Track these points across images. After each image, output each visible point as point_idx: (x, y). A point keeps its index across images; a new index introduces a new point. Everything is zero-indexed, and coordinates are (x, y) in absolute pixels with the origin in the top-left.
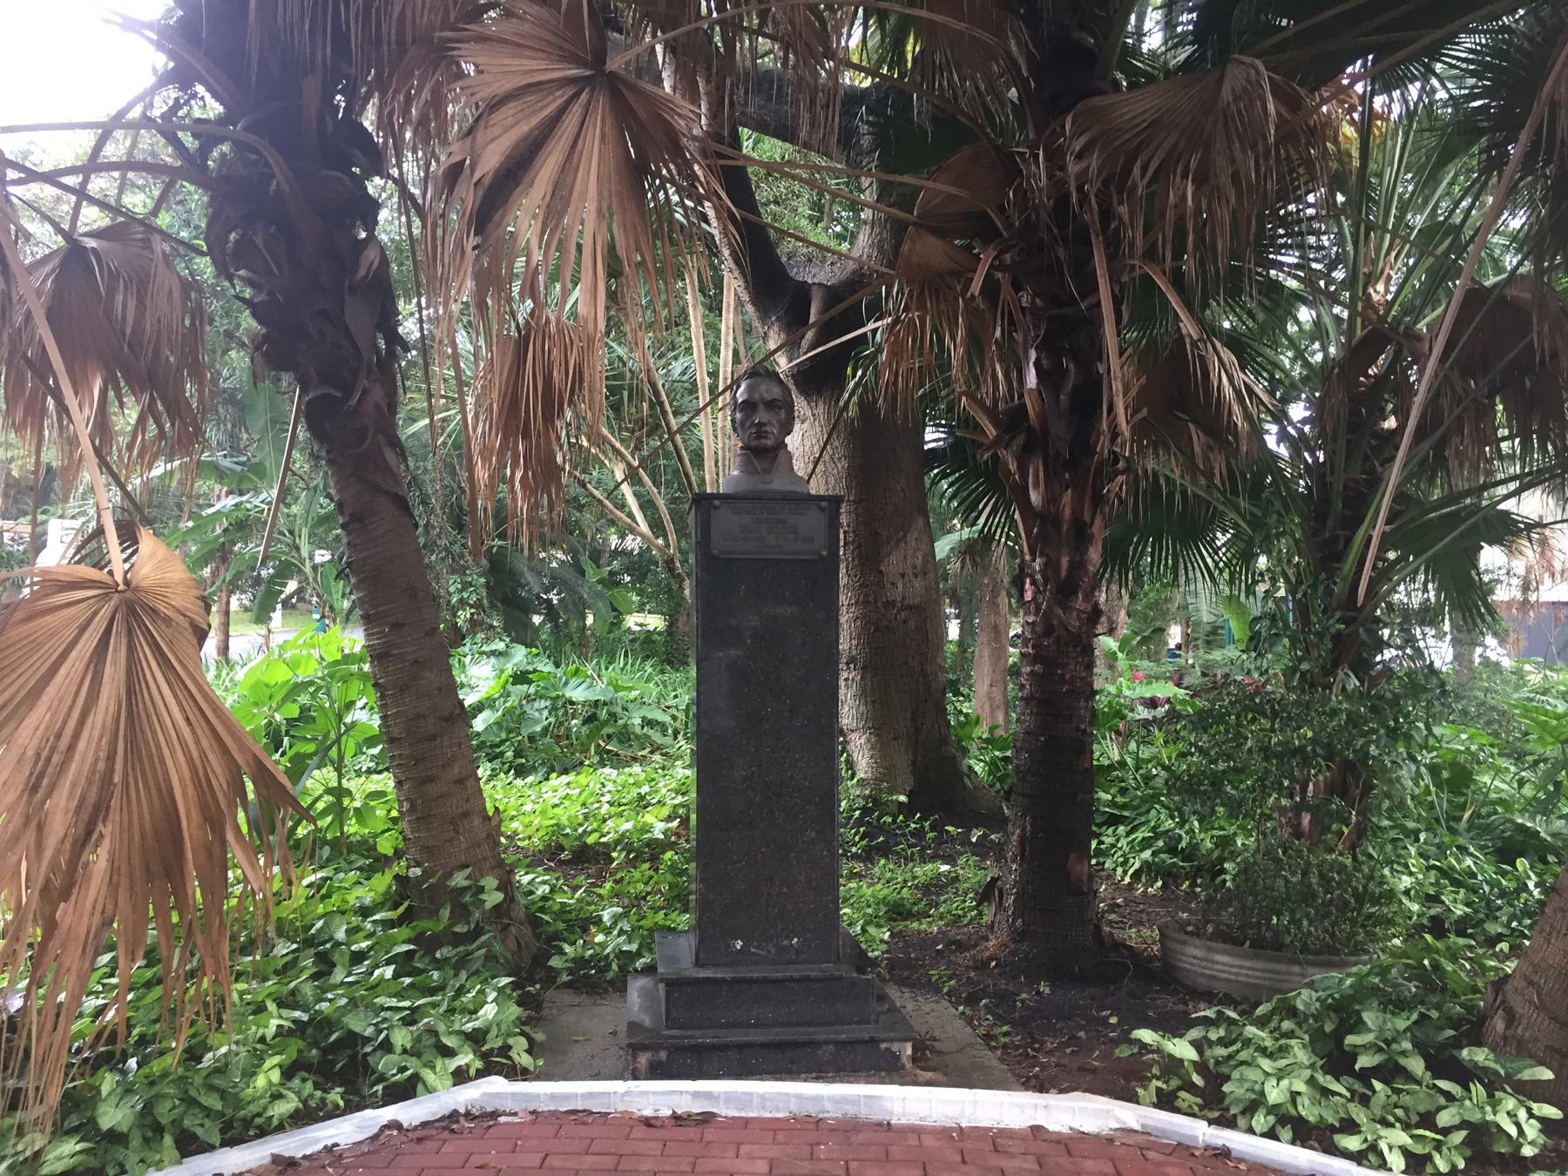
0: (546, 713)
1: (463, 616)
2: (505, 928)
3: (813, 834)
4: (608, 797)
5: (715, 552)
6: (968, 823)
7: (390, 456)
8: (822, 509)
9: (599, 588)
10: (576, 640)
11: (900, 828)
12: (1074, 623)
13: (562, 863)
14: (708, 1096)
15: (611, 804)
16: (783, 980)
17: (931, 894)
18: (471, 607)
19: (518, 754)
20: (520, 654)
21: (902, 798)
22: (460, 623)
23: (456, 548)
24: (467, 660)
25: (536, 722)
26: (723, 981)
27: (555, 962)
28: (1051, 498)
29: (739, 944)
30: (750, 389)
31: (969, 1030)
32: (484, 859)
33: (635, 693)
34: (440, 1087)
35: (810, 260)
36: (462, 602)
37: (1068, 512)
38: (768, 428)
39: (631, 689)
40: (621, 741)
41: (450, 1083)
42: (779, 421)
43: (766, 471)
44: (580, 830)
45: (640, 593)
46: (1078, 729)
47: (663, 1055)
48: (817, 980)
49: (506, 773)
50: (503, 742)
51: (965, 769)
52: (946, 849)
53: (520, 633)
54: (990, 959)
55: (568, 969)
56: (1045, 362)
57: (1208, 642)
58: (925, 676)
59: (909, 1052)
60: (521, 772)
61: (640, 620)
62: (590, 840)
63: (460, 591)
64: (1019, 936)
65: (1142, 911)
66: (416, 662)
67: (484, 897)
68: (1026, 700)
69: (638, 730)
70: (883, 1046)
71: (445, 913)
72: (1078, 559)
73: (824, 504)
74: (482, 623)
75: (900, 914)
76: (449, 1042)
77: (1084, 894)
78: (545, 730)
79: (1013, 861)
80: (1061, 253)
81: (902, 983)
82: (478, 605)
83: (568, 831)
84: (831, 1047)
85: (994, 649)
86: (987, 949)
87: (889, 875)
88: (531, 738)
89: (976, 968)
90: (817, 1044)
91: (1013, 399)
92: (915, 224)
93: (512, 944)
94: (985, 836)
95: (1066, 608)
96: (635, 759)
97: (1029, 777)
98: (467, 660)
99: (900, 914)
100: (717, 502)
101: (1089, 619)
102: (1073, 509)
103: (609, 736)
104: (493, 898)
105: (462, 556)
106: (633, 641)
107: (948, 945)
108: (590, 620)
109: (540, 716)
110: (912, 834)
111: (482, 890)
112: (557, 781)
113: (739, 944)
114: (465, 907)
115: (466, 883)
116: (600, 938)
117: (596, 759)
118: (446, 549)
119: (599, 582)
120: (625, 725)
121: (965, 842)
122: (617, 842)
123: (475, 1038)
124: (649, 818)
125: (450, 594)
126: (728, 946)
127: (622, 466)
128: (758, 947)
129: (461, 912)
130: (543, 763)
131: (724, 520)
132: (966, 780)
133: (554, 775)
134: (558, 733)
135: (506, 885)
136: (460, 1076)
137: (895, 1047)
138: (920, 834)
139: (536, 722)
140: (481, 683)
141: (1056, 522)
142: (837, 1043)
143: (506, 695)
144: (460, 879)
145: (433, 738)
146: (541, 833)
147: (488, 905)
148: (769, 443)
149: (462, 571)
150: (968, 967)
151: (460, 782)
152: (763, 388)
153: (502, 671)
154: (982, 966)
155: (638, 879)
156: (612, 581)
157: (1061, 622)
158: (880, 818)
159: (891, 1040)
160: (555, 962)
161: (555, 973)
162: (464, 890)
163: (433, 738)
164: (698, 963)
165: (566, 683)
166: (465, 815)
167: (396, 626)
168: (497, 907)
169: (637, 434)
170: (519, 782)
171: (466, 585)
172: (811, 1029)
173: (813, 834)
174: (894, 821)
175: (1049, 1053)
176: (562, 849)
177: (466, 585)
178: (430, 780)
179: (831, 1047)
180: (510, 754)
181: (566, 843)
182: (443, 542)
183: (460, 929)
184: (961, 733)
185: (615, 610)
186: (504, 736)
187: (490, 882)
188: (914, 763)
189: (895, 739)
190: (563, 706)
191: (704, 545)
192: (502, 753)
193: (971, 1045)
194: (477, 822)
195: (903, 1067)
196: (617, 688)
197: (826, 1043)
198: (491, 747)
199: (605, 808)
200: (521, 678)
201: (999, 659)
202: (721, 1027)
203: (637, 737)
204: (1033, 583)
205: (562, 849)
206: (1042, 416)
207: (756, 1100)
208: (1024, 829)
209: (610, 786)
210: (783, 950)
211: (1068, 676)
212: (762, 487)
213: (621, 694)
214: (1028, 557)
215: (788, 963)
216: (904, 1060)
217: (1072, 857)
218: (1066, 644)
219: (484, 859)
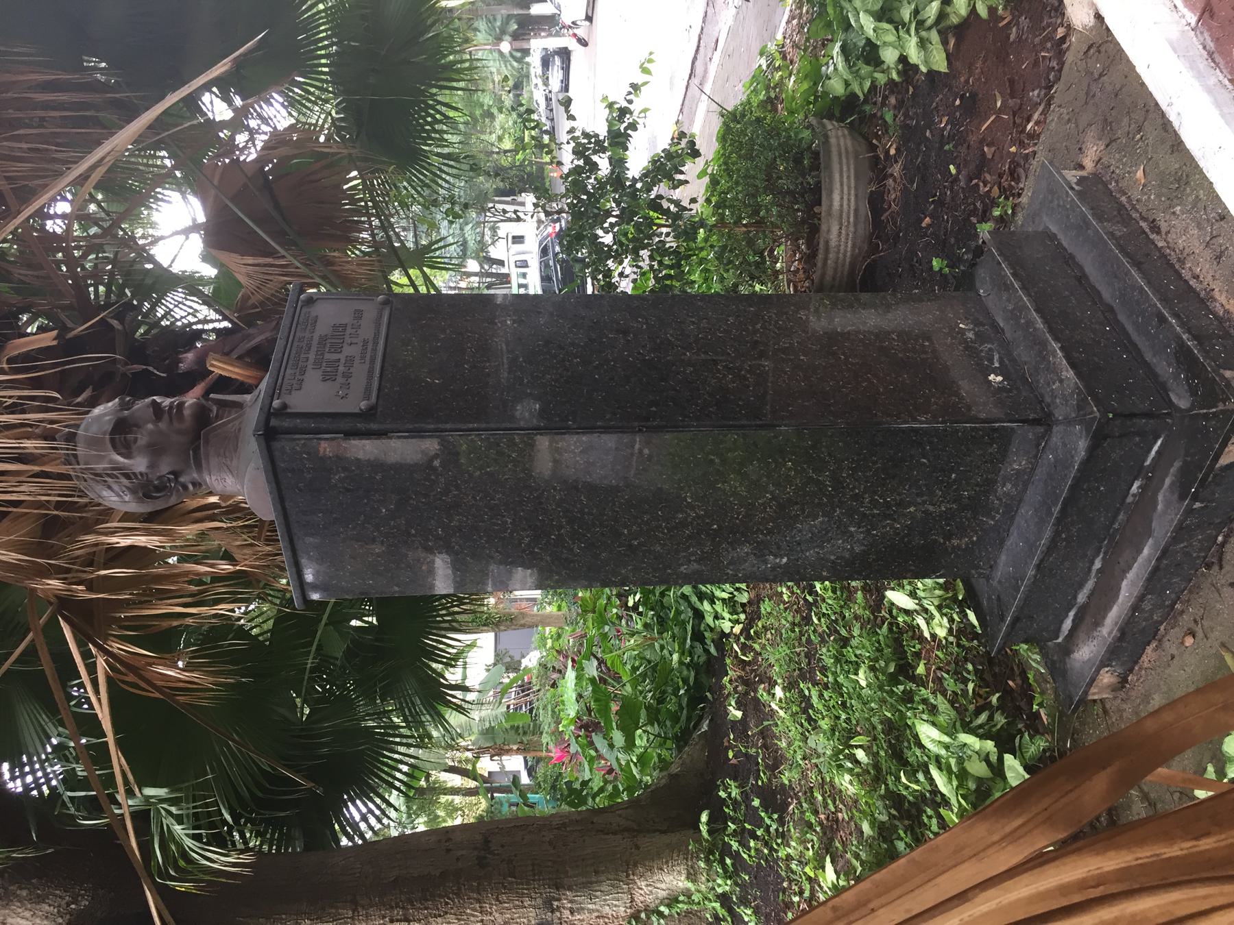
58: (564, 825)
189: (637, 848)
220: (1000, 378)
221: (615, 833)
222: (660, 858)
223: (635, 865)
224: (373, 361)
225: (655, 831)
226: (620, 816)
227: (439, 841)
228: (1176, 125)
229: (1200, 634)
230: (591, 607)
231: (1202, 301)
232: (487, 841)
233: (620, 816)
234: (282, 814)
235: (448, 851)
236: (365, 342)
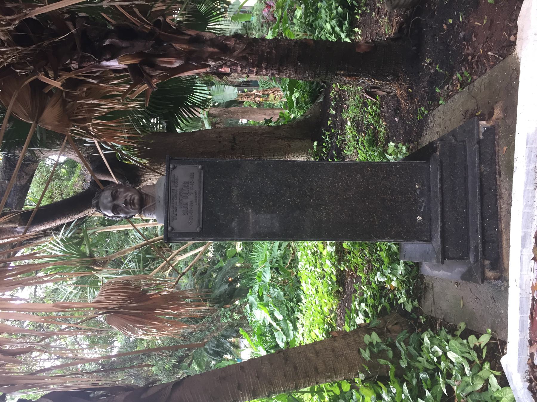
0: (275, 290)
1: (236, 316)
2: (388, 330)
3: (359, 176)
4: (313, 269)
5: (198, 230)
6: (325, 115)
7: (151, 392)
8: (174, 168)
9: (227, 261)
10: (245, 271)
11: (328, 145)
12: (242, 46)
13: (344, 290)
14: (524, 239)
15: (316, 267)
16: (442, 194)
17: (362, 129)
18: (233, 313)
19: (292, 301)
20: (252, 298)
21: (315, 144)
22: (238, 318)
23: (210, 319)
24: (254, 320)
25: (279, 294)
26: (443, 228)
27: (409, 308)
28: (178, 54)
29: (419, 218)
30: (106, 208)
31: (456, 96)
32: (355, 341)
33: (268, 253)
34: (510, 395)
35: (84, 180)
36: (230, 317)
37: (185, 46)
38: (128, 198)
39: (266, 255)
40: (286, 258)
41: (508, 389)
42: (125, 192)
43: (153, 199)
44: (330, 283)
45: (228, 247)
46: (294, 46)
47: (487, 262)
48: (442, 175)
49: (299, 306)
50: (287, 307)
51: (303, 117)
52: (338, 124)
53: (243, 293)
54: (407, 92)
55: (412, 302)
56: (108, 57)
57: (249, 29)
58: (263, 134)
59: (484, 122)
60: (299, 300)
61: (239, 246)
62: (335, 279)
63: (227, 318)
64: (396, 78)
65: (371, 34)
66: (258, 377)
67: (375, 343)
68: (280, 72)
69: (282, 252)
70: (481, 137)
71: (382, 361)
72: (209, 43)
73: (171, 167)
74: (239, 309)
75: (374, 141)
76: (479, 386)
77: (375, 45)
78: (282, 290)
79: (358, 81)
80: (46, 43)
81: (419, 135)
82: (232, 311)
83: (330, 288)
84: (482, 166)
85: (251, 113)
86: (401, 94)
87: (352, 148)
88: (285, 295)
89: (412, 99)
90: (481, 173)
91: (128, 76)
92: (37, 123)
93: (397, 328)
94: (333, 108)
95: (234, 50)
96: (293, 254)
97: (318, 71)
98: (254, 320)
99: (374, 141)
100: (169, 229)
101: (239, 39)
102: (184, 44)
103: (284, 263)
104: (375, 338)
105: (213, 317)
106: (246, 249)
107: (396, 115)
108: (238, 265)
109: (277, 292)
110: (331, 139)
111: (371, 343)
112: (304, 286)
113: (419, 218)
114: (379, 352)
115: (368, 351)
116: (394, 284)
117: (294, 270)
118: (210, 323)
119: (224, 261)
120: (280, 257)
121: (335, 116)
122: (336, 267)
123: (476, 368)
124: (325, 253)
125: (228, 321)
126: (420, 224)
127: (177, 257)
128: (421, 207)
129: (382, 354)
130: (296, 291)
131: (180, 223)
132: (307, 117)
133: (301, 288)
134: (283, 285)
135: (366, 329)
136: (504, 382)
137: (482, 130)
138: (331, 136)
139: (279, 294)
140: (263, 316)
141: (190, 52)
142: (480, 163)
143: (267, 305)
144: (366, 355)
145: (295, 368)
146: (331, 300)
147: (379, 340)
148: (137, 197)
149: (219, 317)
150: (411, 103)
151: (317, 353)
152: (105, 201)
153: (258, 307)
154: (411, 97)
155: (356, 259)
156: (224, 257)
157: (240, 53)
158: (324, 153)
159: (479, 132)
160: (409, 308)
161: (414, 309)
162: (371, 352)
163: (295, 368)
164: (429, 241)
165: (264, 281)
166: (333, 350)
167: (239, 387)
168: (380, 335)
169: (165, 251)
170: (303, 301)
171: (224, 316)
172: (470, 178)
173: (359, 176)
174: (325, 147)
175: (475, 49)
176: (338, 291)
177: (224, 316)
178: (316, 369)
179: (482, 166)
180: (292, 304)
181: (335, 289)
182: (207, 324)
183: (391, 354)
184: (287, 120)
185: (235, 256)
186: (284, 306)
187: (367, 338)
188: (300, 139)
189: (290, 147)
190: (273, 283)
191: (192, 236)
192: (291, 307)
193: (470, 92)
194: (337, 344)
195: (493, 126)
196: (266, 261)
197: (480, 169)
198: (289, 311)
199: (319, 270)
200: (261, 299)
201: (255, 112)
202: (467, 229)
203: (285, 252)
204: (221, 67)
205: (338, 291)
206: (133, 57)
207: (527, 210)
208: (344, 75)
209: (307, 266)
210: (422, 194)
211: (268, 50)
212: (162, 202)
213: (268, 258)
214: (208, 69)
215: (429, 191)
216: (489, 125)
217: (358, 50)
218: (252, 50)
219: (355, 341)
220: (421, 218)
221: (282, 139)
222: (298, 153)
223: (288, 154)
224: (199, 204)
225: (297, 139)
226: (284, 131)
227: (217, 137)
228: (514, 170)
229: (459, 288)
230: (281, 6)
231: (498, 219)
232: (234, 139)
233: (284, 131)
234: (142, 2)
235: (220, 142)
236: (196, 192)
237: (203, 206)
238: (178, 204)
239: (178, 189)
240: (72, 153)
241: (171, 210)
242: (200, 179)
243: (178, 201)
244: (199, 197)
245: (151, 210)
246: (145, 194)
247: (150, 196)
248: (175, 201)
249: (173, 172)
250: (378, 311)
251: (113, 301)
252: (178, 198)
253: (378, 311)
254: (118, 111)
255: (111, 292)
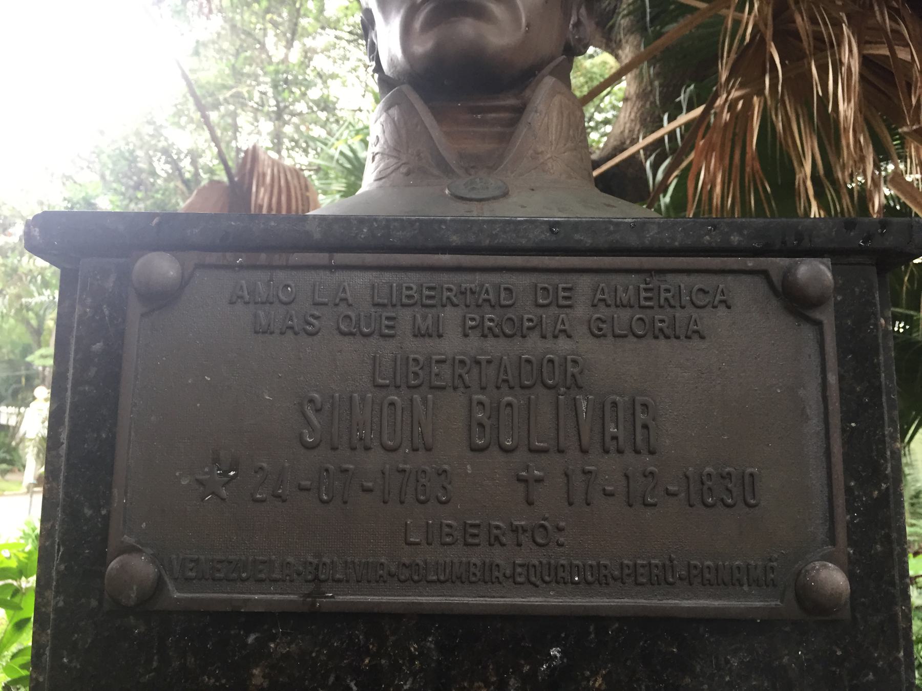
8: (796, 302)
73: (815, 272)
237: (396, 616)
238: (416, 348)
239: (584, 346)
240: (633, 115)
241: (361, 279)
242: (696, 578)
243: (452, 344)
244: (489, 576)
245: (411, 153)
246: (520, 111)
247: (505, 138)
248: (451, 316)
249: (744, 292)
250: (702, 108)
251: (261, 197)
252: (474, 344)
253: (702, 108)
254: (791, 174)
255: (297, 198)
